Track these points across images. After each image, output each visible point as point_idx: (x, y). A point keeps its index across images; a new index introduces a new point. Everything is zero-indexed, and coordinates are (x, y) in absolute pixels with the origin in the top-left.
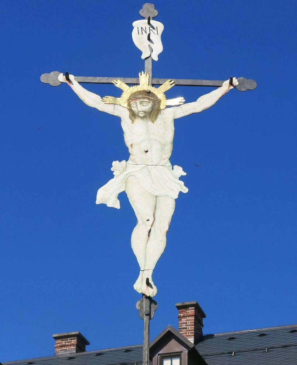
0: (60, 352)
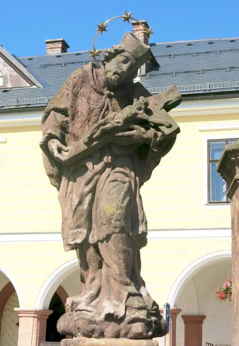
0: (50, 53)
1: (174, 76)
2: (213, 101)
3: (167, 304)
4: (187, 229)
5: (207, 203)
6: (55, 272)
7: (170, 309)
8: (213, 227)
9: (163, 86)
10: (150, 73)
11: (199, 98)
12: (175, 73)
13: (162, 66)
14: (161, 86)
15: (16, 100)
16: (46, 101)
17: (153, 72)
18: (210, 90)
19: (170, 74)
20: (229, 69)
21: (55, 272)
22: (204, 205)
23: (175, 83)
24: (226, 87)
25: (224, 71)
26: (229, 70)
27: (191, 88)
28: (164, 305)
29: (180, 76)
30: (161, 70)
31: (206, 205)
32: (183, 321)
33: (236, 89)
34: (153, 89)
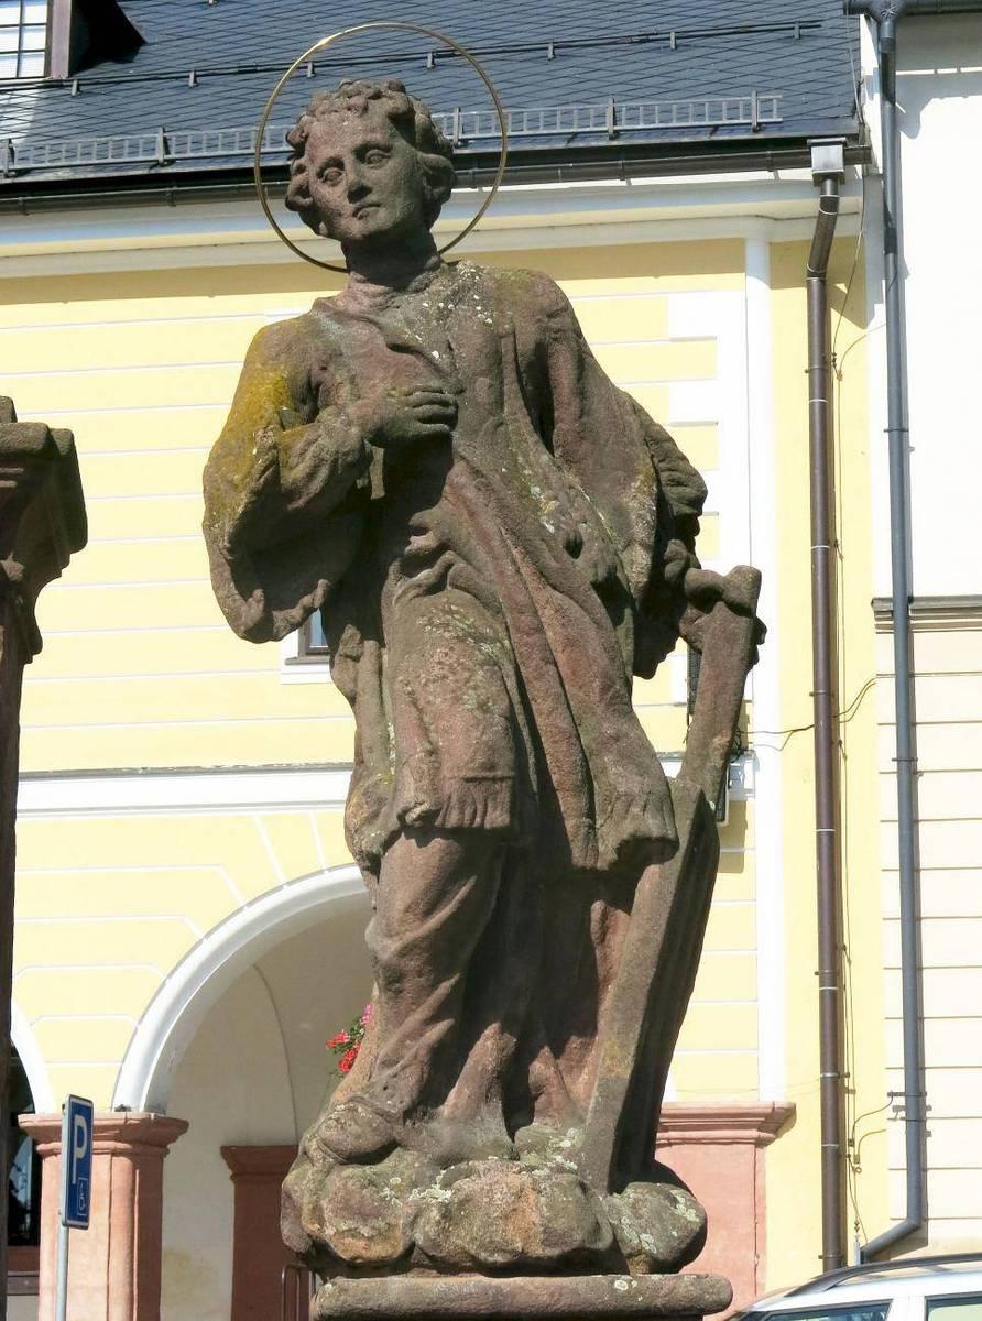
1: (73, 97)
2: (180, 209)
3: (74, 1100)
4: (208, 767)
5: (296, 655)
6: (139, 1027)
7: (95, 1123)
8: (323, 760)
9: (121, 133)
10: (87, 74)
11: (558, 168)
12: (555, 48)
13: (155, 44)
14: (116, 134)
15: (159, 137)
16: (748, 115)
17: (109, 69)
18: (617, 134)
19: (177, 78)
20: (434, 58)
21: (139, 1027)
22: (284, 666)
23: (182, 117)
24: (595, 125)
25: (779, 40)
26: (551, 56)
27: (715, 114)
28: (64, 1106)
29: (218, 86)
30: (146, 61)
31: (290, 662)
32: (230, 1172)
33: (569, 141)
34: (141, 141)
